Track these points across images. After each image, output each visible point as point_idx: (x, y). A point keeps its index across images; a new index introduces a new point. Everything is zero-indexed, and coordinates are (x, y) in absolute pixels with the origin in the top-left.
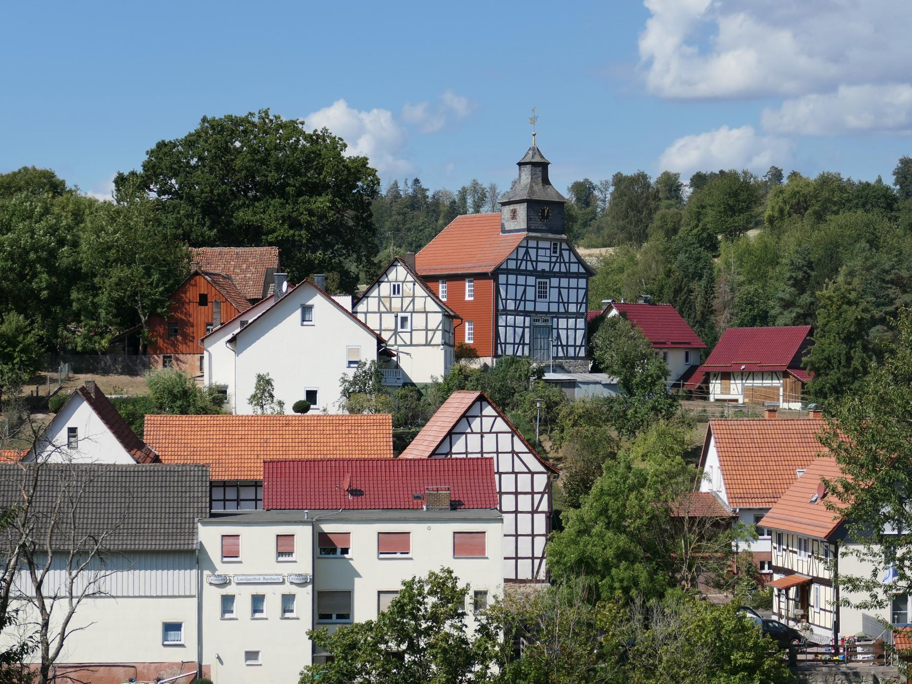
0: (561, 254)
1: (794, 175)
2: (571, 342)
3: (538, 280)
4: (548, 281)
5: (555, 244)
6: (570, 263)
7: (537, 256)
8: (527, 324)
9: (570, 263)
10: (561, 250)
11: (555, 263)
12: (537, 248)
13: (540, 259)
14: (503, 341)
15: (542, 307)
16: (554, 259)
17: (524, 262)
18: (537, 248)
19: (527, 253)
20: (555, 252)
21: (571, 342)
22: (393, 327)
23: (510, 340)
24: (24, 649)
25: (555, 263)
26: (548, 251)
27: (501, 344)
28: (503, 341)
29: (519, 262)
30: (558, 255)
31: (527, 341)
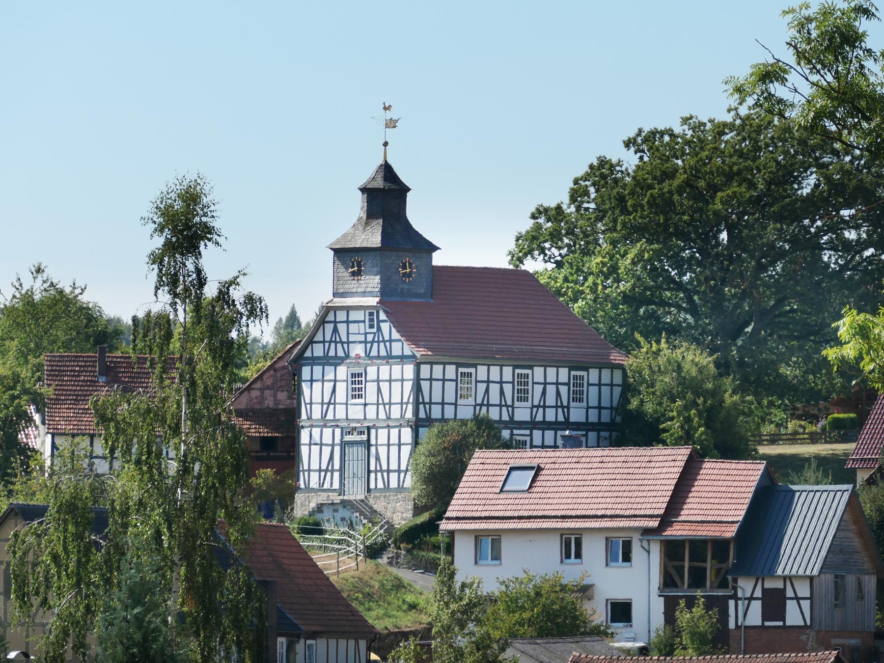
0: (379, 329)
1: (711, 121)
2: (394, 466)
3: (573, 373)
4: (584, 373)
5: (371, 314)
6: (391, 341)
7: (348, 334)
8: (337, 440)
9: (391, 341)
10: (379, 321)
11: (372, 342)
12: (348, 322)
13: (352, 338)
14: (427, 400)
15: (356, 412)
16: (370, 338)
17: (333, 345)
18: (348, 322)
19: (335, 330)
20: (371, 326)
21: (394, 466)
22: (454, 378)
23: (315, 466)
24: (792, 105)
25: (372, 342)
26: (362, 325)
27: (424, 403)
28: (306, 468)
29: (327, 345)
30: (375, 330)
31: (337, 466)
